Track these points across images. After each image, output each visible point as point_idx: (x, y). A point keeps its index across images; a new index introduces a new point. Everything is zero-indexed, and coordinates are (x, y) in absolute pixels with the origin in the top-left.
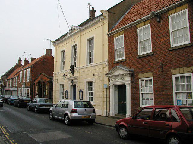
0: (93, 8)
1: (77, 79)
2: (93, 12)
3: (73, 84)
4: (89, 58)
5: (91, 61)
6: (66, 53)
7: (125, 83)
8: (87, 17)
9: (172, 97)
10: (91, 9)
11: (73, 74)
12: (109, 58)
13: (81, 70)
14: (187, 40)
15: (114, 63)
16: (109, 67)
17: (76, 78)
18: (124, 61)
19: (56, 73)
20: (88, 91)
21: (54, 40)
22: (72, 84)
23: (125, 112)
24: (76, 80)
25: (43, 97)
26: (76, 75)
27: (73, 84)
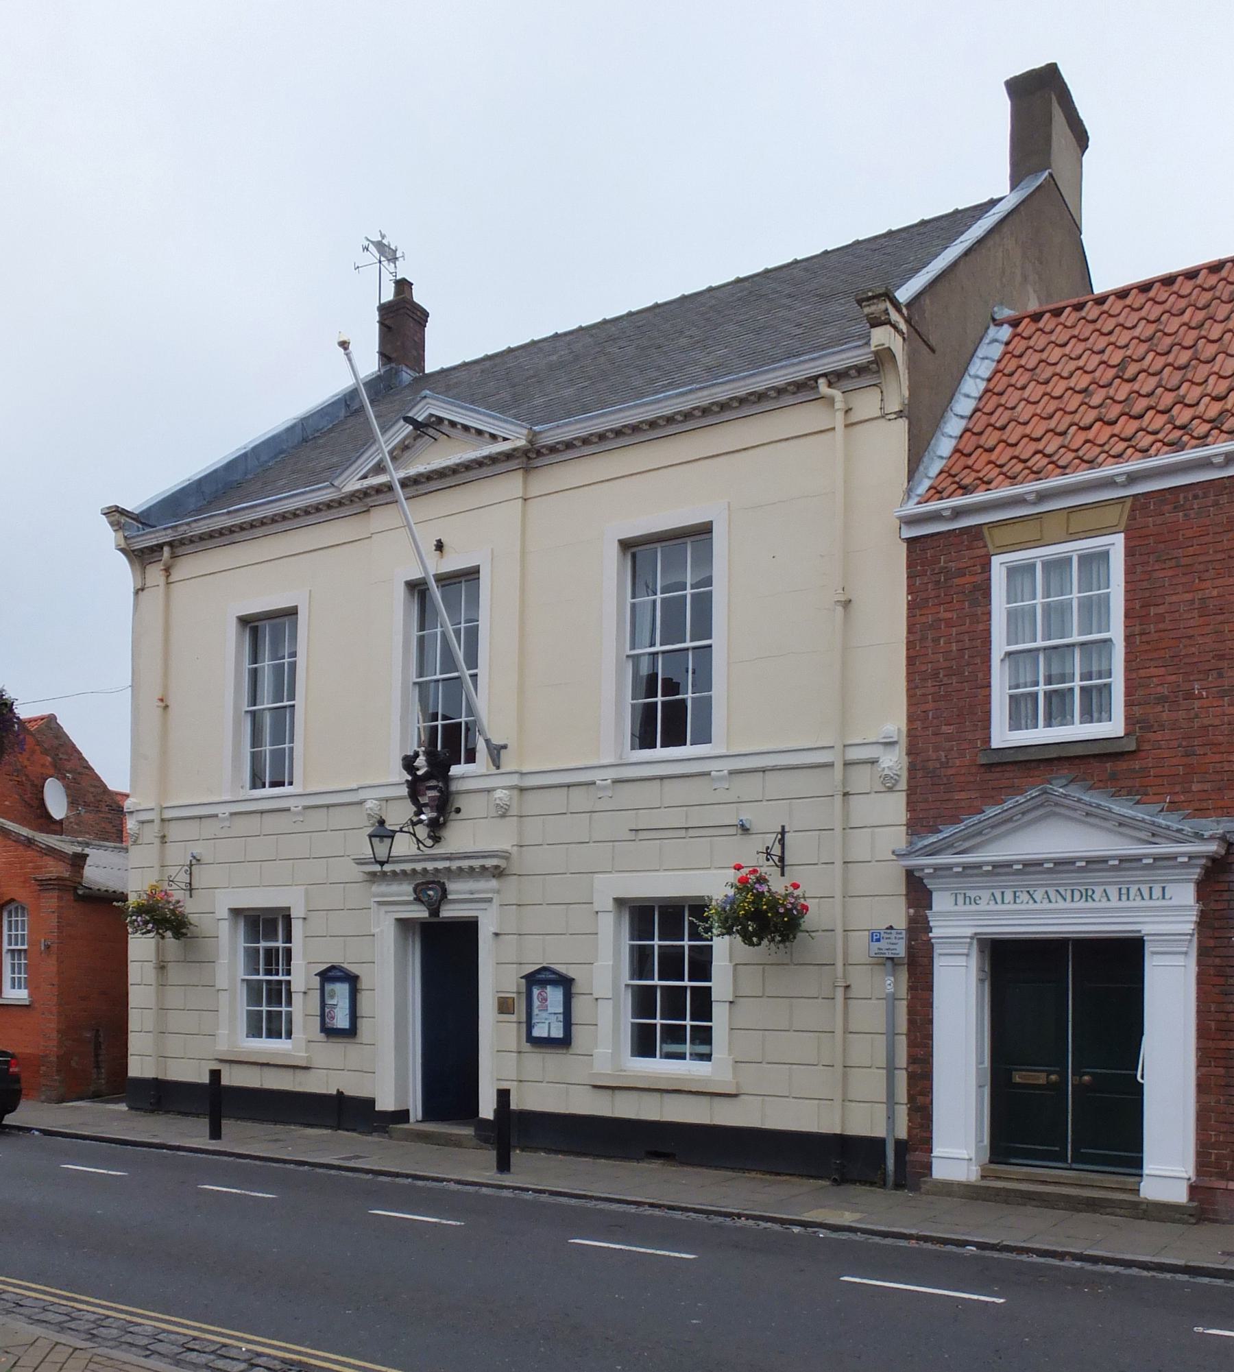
0: (403, 286)
1: (498, 873)
2: (402, 321)
3: (435, 912)
4: (247, 750)
5: (269, 771)
6: (312, 648)
7: (1146, 929)
8: (329, 361)
9: (1204, 1070)
10: (389, 295)
11: (436, 828)
12: (911, 719)
13: (174, 831)
14: (1095, 715)
15: (983, 760)
16: (911, 792)
17: (489, 863)
18: (1122, 754)
19: (163, 808)
20: (625, 978)
21: (134, 502)
22: (421, 913)
23: (1116, 1129)
24: (494, 883)
25: (1213, 906)
26: (462, 837)
27: (435, 912)
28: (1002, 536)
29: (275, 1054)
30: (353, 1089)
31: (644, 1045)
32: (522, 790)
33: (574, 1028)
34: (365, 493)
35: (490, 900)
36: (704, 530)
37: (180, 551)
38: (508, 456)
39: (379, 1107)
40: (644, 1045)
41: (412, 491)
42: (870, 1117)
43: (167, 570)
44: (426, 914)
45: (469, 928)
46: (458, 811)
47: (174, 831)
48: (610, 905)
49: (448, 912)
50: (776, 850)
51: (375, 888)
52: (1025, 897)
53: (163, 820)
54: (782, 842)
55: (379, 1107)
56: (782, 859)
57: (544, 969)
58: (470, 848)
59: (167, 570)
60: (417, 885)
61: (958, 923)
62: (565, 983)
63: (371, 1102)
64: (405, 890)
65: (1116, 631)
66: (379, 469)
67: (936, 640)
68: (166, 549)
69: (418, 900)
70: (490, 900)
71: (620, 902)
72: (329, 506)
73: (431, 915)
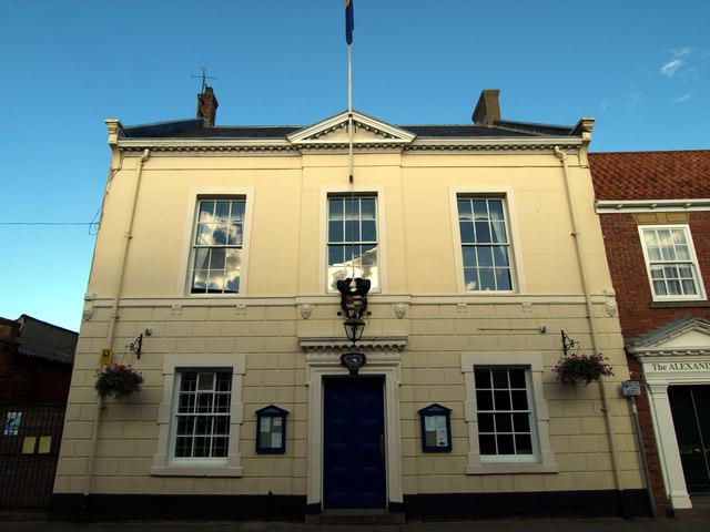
1: (401, 349)
16: (621, 318)
24: (398, 355)
28: (641, 218)
29: (506, 464)
30: (282, 488)
31: (487, 447)
32: (410, 304)
33: (255, 437)
34: (304, 146)
35: (395, 365)
36: (375, 194)
37: (153, 154)
38: (398, 145)
39: (309, 502)
40: (183, 449)
41: (357, 151)
42: (632, 479)
43: (143, 161)
44: (348, 373)
45: (379, 381)
46: (369, 313)
47: (125, 314)
48: (172, 371)
49: (363, 371)
50: (137, 346)
51: (309, 356)
52: (686, 366)
53: (118, 307)
54: (140, 342)
55: (309, 502)
56: (139, 350)
57: (436, 405)
58: (385, 334)
59: (143, 161)
60: (344, 355)
61: (659, 377)
62: (446, 412)
63: (304, 498)
64: (335, 357)
65: (694, 259)
66: (314, 137)
67: (620, 255)
68: (147, 150)
69: (344, 364)
70: (395, 365)
71: (178, 370)
72: (283, 148)
73: (351, 373)
